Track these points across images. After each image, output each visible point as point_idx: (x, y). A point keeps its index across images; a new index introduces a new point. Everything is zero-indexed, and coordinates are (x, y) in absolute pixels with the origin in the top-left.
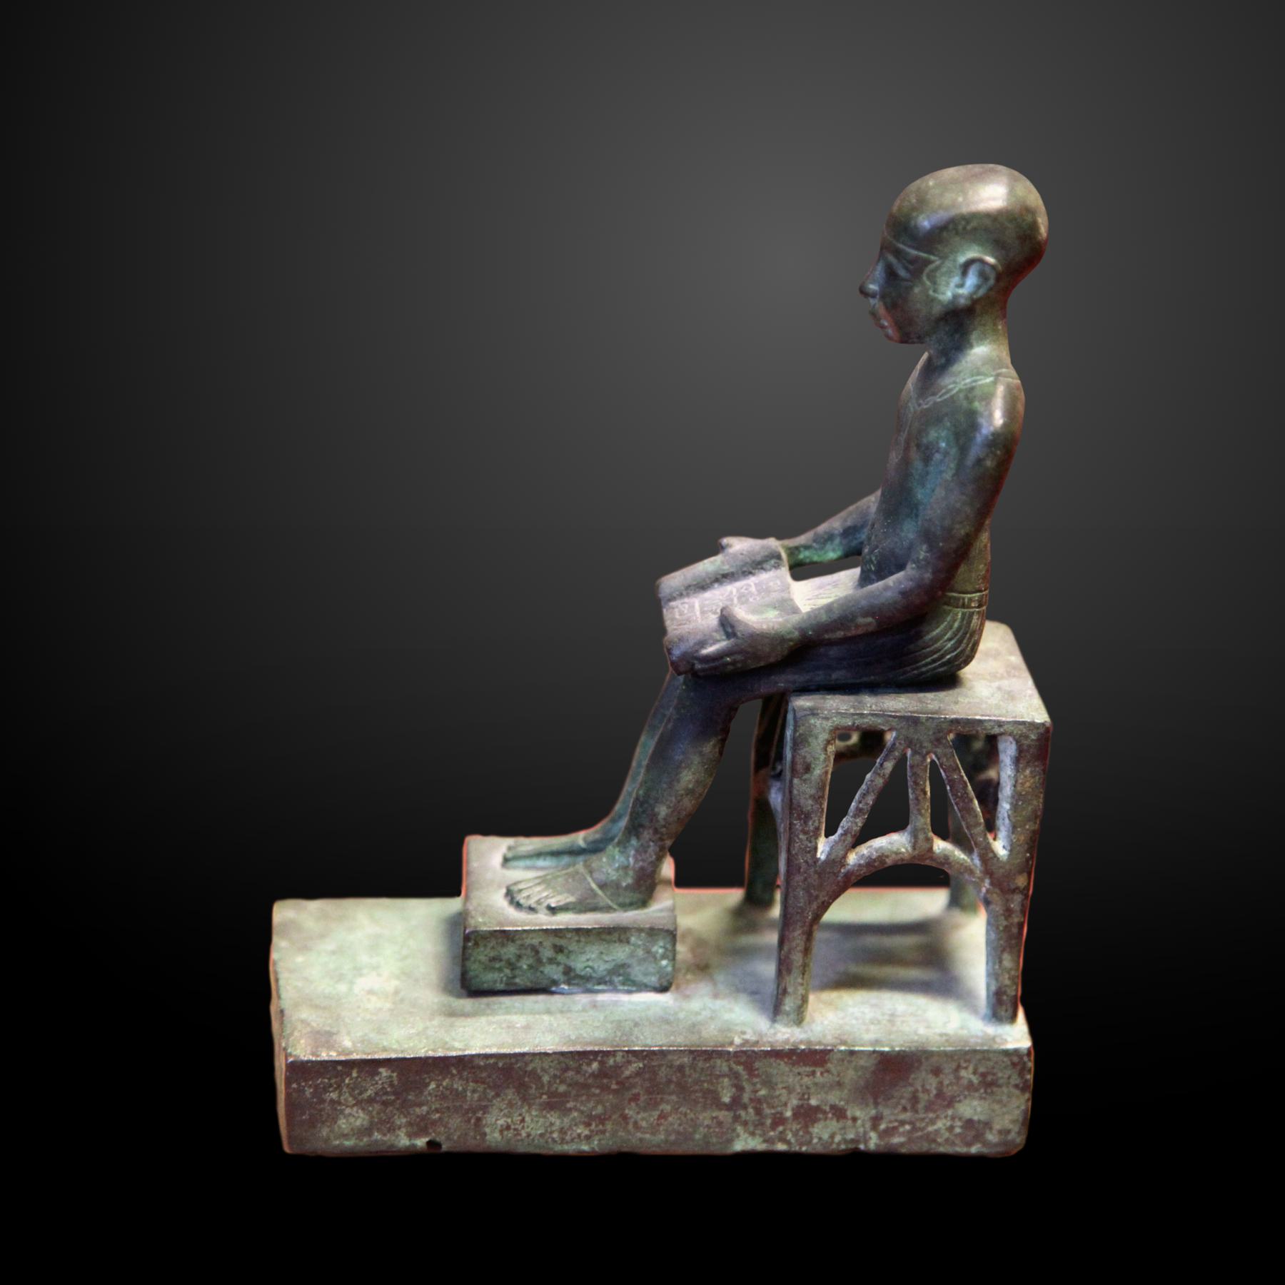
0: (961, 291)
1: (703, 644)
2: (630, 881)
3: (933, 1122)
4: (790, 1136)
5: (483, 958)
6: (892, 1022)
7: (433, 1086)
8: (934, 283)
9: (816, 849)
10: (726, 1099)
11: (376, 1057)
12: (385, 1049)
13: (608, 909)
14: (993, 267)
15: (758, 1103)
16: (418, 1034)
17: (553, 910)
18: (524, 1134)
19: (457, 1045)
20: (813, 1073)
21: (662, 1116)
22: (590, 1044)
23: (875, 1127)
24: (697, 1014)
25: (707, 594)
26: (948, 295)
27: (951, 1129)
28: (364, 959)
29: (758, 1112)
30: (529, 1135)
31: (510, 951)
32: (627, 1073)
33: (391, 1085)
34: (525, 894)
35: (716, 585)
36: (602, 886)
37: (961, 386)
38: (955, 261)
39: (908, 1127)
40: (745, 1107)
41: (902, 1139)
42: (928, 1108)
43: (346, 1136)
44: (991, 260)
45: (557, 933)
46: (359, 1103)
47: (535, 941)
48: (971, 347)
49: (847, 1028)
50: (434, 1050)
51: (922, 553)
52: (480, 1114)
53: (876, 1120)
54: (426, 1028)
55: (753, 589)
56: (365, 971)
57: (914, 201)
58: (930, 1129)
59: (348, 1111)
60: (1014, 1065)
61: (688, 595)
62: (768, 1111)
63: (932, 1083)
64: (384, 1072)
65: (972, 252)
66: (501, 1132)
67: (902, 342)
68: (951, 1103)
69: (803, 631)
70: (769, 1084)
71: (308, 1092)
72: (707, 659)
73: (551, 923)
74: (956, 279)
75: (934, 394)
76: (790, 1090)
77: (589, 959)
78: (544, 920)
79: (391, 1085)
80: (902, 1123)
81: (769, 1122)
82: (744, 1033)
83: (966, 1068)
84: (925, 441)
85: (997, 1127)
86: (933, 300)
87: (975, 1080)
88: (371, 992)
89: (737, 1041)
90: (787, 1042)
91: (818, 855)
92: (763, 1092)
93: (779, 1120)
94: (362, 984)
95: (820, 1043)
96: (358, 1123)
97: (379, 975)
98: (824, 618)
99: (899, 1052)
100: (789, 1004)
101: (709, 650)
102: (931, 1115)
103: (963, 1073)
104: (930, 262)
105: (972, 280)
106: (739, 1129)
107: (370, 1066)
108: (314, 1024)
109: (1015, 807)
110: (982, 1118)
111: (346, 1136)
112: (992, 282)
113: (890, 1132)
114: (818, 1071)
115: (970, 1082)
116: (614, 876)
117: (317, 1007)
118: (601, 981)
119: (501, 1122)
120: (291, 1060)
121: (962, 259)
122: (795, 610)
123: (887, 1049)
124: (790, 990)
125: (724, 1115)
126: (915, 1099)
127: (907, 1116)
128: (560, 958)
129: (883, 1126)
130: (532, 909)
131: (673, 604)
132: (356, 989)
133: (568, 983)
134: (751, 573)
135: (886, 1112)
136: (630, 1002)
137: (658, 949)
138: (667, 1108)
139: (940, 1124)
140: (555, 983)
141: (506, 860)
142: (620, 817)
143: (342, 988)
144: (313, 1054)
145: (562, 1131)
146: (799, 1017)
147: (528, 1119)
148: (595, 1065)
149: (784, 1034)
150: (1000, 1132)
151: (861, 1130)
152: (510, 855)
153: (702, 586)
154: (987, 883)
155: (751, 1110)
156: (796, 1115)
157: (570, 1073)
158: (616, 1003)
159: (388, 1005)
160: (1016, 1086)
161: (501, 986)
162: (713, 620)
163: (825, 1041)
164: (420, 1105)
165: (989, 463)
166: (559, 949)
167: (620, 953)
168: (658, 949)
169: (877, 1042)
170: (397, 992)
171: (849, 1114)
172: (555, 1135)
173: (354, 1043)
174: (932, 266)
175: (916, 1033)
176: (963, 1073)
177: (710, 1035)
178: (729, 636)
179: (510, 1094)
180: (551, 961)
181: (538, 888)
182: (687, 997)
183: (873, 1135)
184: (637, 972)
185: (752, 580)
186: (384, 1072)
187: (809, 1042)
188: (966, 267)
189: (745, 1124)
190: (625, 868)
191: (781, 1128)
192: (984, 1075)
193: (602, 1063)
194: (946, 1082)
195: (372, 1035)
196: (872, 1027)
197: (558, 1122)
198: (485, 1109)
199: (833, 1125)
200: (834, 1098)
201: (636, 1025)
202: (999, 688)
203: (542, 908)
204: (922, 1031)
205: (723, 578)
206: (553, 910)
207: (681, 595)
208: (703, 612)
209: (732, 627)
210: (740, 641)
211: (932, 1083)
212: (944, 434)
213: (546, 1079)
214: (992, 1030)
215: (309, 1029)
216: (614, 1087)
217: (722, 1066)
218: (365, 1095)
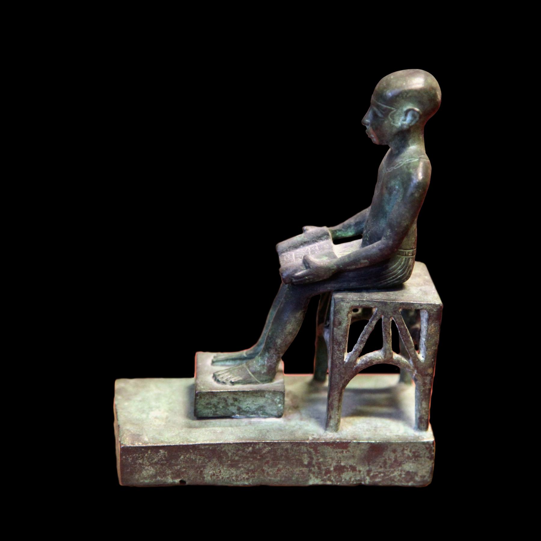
0: (404, 123)
1: (296, 271)
2: (265, 371)
3: (393, 472)
4: (332, 478)
5: (203, 403)
6: (375, 430)
7: (182, 457)
8: (393, 119)
9: (343, 357)
10: (306, 463)
11: (158, 445)
12: (162, 442)
13: (256, 383)
14: (418, 112)
15: (319, 464)
16: (176, 435)
17: (233, 383)
18: (221, 477)
19: (192, 440)
20: (342, 452)
21: (279, 470)
22: (248, 439)
23: (368, 475)
24: (294, 427)
25: (298, 250)
26: (399, 124)
27: (400, 475)
28: (153, 404)
29: (319, 468)
30: (223, 478)
31: (215, 400)
32: (264, 452)
33: (165, 457)
34: (221, 376)
35: (301, 246)
36: (254, 373)
37: (405, 162)
38: (402, 110)
39: (382, 475)
40: (314, 466)
41: (380, 480)
42: (391, 467)
43: (145, 478)
44: (417, 109)
45: (234, 393)
46: (151, 464)
47: (225, 396)
48: (409, 146)
49: (357, 433)
50: (183, 442)
51: (388, 233)
52: (202, 469)
53: (369, 472)
54: (179, 433)
55: (317, 248)
56: (154, 409)
57: (385, 84)
58: (392, 475)
59: (146, 468)
60: (427, 448)
61: (290, 251)
62: (323, 468)
63: (392, 456)
64: (162, 451)
65: (409, 106)
66: (211, 476)
68: (400, 464)
69: (338, 266)
70: (324, 456)
71: (130, 460)
72: (298, 277)
73: (232, 389)
74: (403, 118)
75: (393, 166)
76: (332, 459)
77: (248, 404)
78: (229, 387)
79: (165, 457)
80: (380, 473)
81: (324, 472)
82: (313, 435)
83: (407, 450)
84: (389, 186)
85: (420, 474)
86: (393, 126)
87: (411, 454)
88: (156, 418)
89: (310, 438)
90: (331, 438)
91: (345, 360)
92: (321, 460)
93: (328, 472)
94: (153, 414)
95: (345, 439)
96: (151, 473)
97: (160, 411)
98: (347, 260)
99: (378, 443)
100: (332, 423)
101: (299, 274)
102: (392, 469)
103: (405, 452)
104: (392, 110)
105: (409, 118)
106: (311, 475)
107: (156, 449)
108: (132, 431)
109: (427, 340)
110: (414, 471)
111: (145, 478)
112: (418, 119)
113: (375, 476)
114: (345, 451)
115: (409, 455)
116: (258, 369)
117: (133, 424)
118: (253, 413)
119: (211, 472)
120: (122, 446)
121: (405, 109)
122: (335, 257)
123: (373, 442)
124: (333, 417)
125: (305, 470)
126: (385, 463)
127: (382, 470)
128: (236, 403)
129: (372, 474)
130: (224, 383)
131: (283, 254)
132: (150, 417)
133: (239, 414)
134: (316, 241)
135: (373, 468)
136: (265, 422)
137: (277, 400)
138: (281, 466)
139: (396, 473)
140: (234, 414)
141: (213, 362)
143: (144, 416)
144: (132, 444)
145: (237, 476)
146: (336, 428)
147: (222, 471)
148: (251, 449)
149: (330, 435)
150: (421, 477)
151: (363, 476)
152: (215, 360)
153: (296, 247)
154: (415, 372)
155: (316, 468)
156: (335, 469)
157: (240, 452)
158: (259, 422)
159: (163, 423)
160: (428, 457)
161: (211, 415)
162: (300, 261)
163: (347, 438)
164: (177, 465)
165: (416, 195)
166: (235, 400)
167: (261, 401)
168: (277, 400)
169: (369, 439)
170: (167, 418)
171: (357, 469)
172: (234, 478)
173: (149, 439)
174: (392, 112)
175: (385, 435)
176: (405, 452)
177: (299, 436)
178: (307, 268)
179: (215, 460)
180: (232, 405)
181: (227, 374)
182: (289, 420)
183: (368, 478)
184: (268, 409)
185: (316, 244)
186: (162, 451)
187: (341, 439)
188: (407, 113)
189: (314, 473)
190: (263, 365)
191: (329, 475)
192: (414, 453)
193: (253, 448)
194: (398, 456)
195: (157, 436)
196: (367, 432)
197: (235, 473)
198: (204, 467)
199: (351, 474)
200: (351, 462)
201: (268, 431)
202: (421, 290)
203: (228, 382)
204: (388, 434)
205: (304, 243)
206: (233, 383)
207: (287, 251)
208: (296, 258)
209: (308, 264)
210: (311, 270)
211: (392, 456)
212: (397, 183)
213: (230, 454)
214: (417, 434)
215: (130, 433)
216: (259, 457)
217: (304, 449)
218: (154, 461)
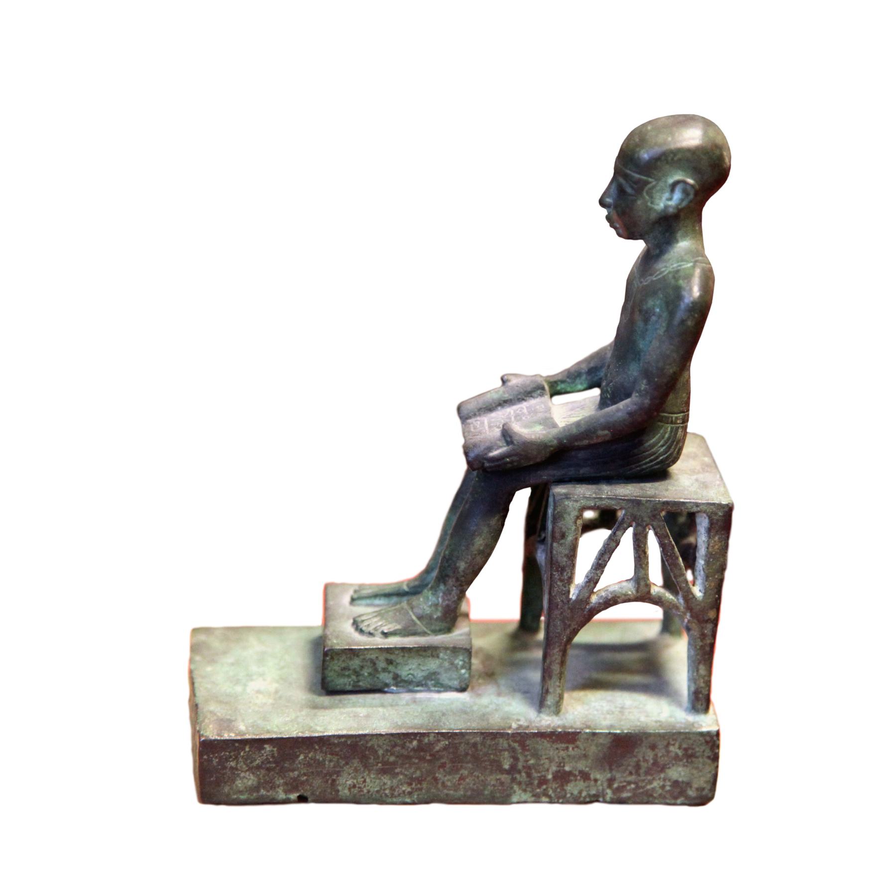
0: (670, 203)
1: (490, 449)
2: (439, 614)
3: (650, 782)
5: (336, 668)
6: (622, 712)
7: (302, 757)
8: (652, 197)
9: (569, 592)
10: (506, 767)
11: (262, 737)
12: (268, 732)
13: (424, 634)
14: (692, 186)
15: (528, 769)
16: (291, 721)
17: (385, 635)
18: (365, 791)
19: (319, 728)
20: (567, 748)
21: (462, 778)
22: (411, 728)
23: (610, 786)
24: (486, 707)
25: (493, 415)
26: (661, 205)
27: (663, 787)
28: (254, 668)
29: (529, 775)
30: (369, 792)
31: (356, 663)
32: (437, 748)
33: (273, 756)
34: (366, 623)
35: (499, 408)
36: (420, 618)
37: (670, 269)
38: (666, 182)
39: (633, 786)
40: (519, 772)
41: (629, 795)
42: (647, 773)
43: (241, 792)
44: (691, 181)
45: (388, 650)
46: (250, 769)
48: (677, 242)
49: (591, 717)
50: (302, 732)
51: (643, 385)
52: (334, 777)
53: (611, 781)
54: (297, 717)
55: (525, 411)
56: (255, 677)
57: (637, 140)
58: (649, 787)
59: (242, 775)
60: (707, 742)
61: (480, 415)
62: (535, 775)
63: (650, 755)
64: (268, 747)
65: (678, 176)
66: (349, 789)
68: (663, 769)
69: (560, 440)
70: (536, 756)
71: (215, 761)
72: (493, 459)
73: (384, 644)
74: (667, 195)
75: (651, 275)
76: (551, 760)
77: (411, 669)
78: (379, 642)
79: (273, 756)
80: (629, 783)
81: (536, 782)
82: (518, 720)
83: (674, 745)
84: (645, 307)
85: (695, 786)
86: (651, 209)
87: (680, 753)
88: (258, 692)
89: (514, 726)
90: (549, 726)
91: (571, 596)
92: (532, 762)
94: (253, 686)
95: (571, 727)
96: (250, 783)
97: (264, 680)
98: (575, 431)
99: (627, 734)
100: (550, 700)
101: (495, 453)
102: (649, 778)
103: (671, 748)
104: (648, 183)
105: (677, 195)
106: (516, 787)
107: (258, 743)
108: (219, 714)
109: (707, 563)
110: (685, 779)
111: (241, 792)
112: (691, 196)
114: (571, 747)
115: (677, 754)
116: (428, 611)
117: (221, 702)
118: (419, 684)
119: (349, 782)
120: (203, 739)
121: (671, 181)
122: (555, 425)
123: (618, 731)
124: (551, 690)
125: (505, 778)
126: (638, 766)
127: (632, 778)
128: (391, 668)
129: (615, 785)
130: (371, 634)
132: (249, 690)
133: (396, 685)
134: (523, 400)
135: (618, 775)
136: (439, 699)
137: (459, 662)
138: (465, 772)
139: (655, 784)
140: (387, 685)
141: (353, 600)
143: (239, 689)
144: (218, 735)
145: (392, 789)
146: (557, 709)
147: (368, 780)
148: (415, 743)
149: (547, 721)
150: (697, 789)
151: (601, 788)
152: (355, 596)
154: (688, 616)
155: (524, 774)
156: (555, 777)
157: (398, 749)
158: (429, 699)
159: (271, 701)
160: (709, 757)
161: (349, 688)
163: (575, 726)
164: (293, 770)
165: (689, 323)
166: (390, 662)
167: (432, 665)
168: (459, 662)
169: (611, 727)
170: (277, 692)
171: (592, 777)
172: (387, 792)
173: (247, 727)
174: (650, 186)
175: (638, 720)
176: (671, 748)
177: (495, 722)
178: (508, 443)
179: (356, 763)
180: (385, 670)
181: (375, 620)
182: (479, 695)
184: (444, 678)
185: (524, 405)
186: (268, 747)
187: (564, 727)
188: (673, 186)
189: (520, 783)
190: (436, 605)
191: (544, 787)
192: (686, 750)
193: (420, 741)
194: (660, 755)
195: (259, 722)
196: (608, 716)
197: (389, 783)
198: (338, 773)
199: (581, 784)
200: (582, 765)
201: (444, 714)
202: (697, 480)
203: (378, 633)
204: (643, 719)
206: (385, 635)
207: (475, 415)
208: (490, 427)
209: (511, 437)
210: (516, 447)
211: (650, 755)
212: (658, 302)
213: (381, 752)
214: (691, 718)
215: (215, 718)
216: (428, 758)
217: (503, 743)
218: (255, 764)
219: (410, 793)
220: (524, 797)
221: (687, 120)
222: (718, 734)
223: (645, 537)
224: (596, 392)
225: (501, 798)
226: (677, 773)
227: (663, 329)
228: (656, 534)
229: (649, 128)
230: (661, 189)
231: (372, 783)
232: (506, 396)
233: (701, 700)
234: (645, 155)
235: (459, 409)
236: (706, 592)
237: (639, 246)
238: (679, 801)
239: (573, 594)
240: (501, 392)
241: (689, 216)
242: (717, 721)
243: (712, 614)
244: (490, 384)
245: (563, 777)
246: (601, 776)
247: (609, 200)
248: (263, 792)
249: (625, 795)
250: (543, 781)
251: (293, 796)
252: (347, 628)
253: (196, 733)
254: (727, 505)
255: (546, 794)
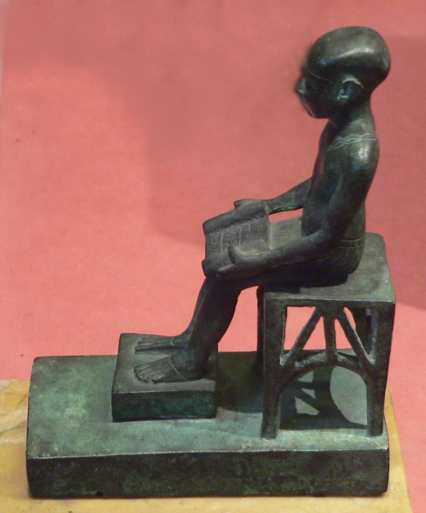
1: (219, 265)
2: (192, 368)
7: (96, 470)
9: (279, 360)
10: (239, 473)
12: (73, 453)
13: (182, 380)
16: (90, 443)
17: (155, 382)
18: (142, 489)
19: (108, 450)
20: (281, 462)
22: (170, 450)
23: (312, 484)
27: (350, 485)
29: (255, 479)
30: (144, 490)
34: (142, 373)
35: (232, 225)
36: (179, 370)
37: (345, 143)
38: (340, 82)
39: (328, 484)
41: (326, 489)
45: (156, 394)
49: (299, 438)
50: (96, 454)
53: (312, 482)
54: (95, 440)
56: (70, 404)
57: (319, 50)
58: (341, 485)
59: (57, 481)
61: (218, 230)
64: (73, 464)
67: (116, 398)
68: (349, 474)
72: (221, 273)
73: (153, 389)
74: (342, 91)
78: (152, 388)
81: (260, 483)
83: (356, 459)
87: (361, 463)
88: (71, 417)
89: (244, 447)
91: (281, 363)
94: (69, 411)
95: (284, 448)
97: (77, 406)
98: (279, 255)
99: (323, 452)
100: (269, 429)
101: (223, 269)
102: (341, 479)
103: (355, 461)
105: (349, 91)
106: (246, 486)
107: (67, 461)
108: (42, 437)
109: (378, 341)
116: (184, 365)
117: (44, 426)
119: (131, 484)
120: (29, 458)
123: (317, 450)
127: (328, 480)
129: (316, 484)
130: (145, 381)
134: (249, 220)
139: (344, 483)
141: (137, 351)
142: (134, 437)
143: (58, 414)
147: (143, 483)
148: (174, 460)
149: (268, 444)
152: (138, 349)
156: (275, 479)
159: (78, 425)
160: (381, 466)
163: (286, 447)
167: (188, 402)
169: (312, 446)
170: (83, 417)
171: (299, 479)
173: (59, 449)
176: (355, 461)
178: (233, 262)
181: (149, 370)
182: (222, 421)
183: (311, 487)
185: (249, 224)
186: (73, 464)
187: (278, 447)
189: (248, 484)
191: (266, 485)
194: (346, 465)
201: (196, 437)
202: (371, 280)
206: (155, 382)
207: (215, 230)
208: (224, 242)
209: (234, 258)
210: (236, 266)
214: (369, 439)
215: (39, 440)
219: (173, 491)
220: (252, 492)
221: (354, 33)
222: (388, 451)
223: (333, 325)
224: (300, 213)
225: (237, 493)
226: (359, 476)
227: (338, 196)
228: (340, 322)
229: (329, 40)
230: (336, 86)
231: (147, 485)
232: (237, 217)
233: (376, 426)
234: (323, 62)
235: (204, 225)
236: (378, 359)
237: (324, 122)
238: (361, 493)
239: (282, 361)
240: (234, 213)
241: (360, 102)
242: (388, 440)
243: (383, 373)
244: (226, 207)
245: (279, 480)
246: (306, 479)
247: (302, 91)
248: (72, 490)
249: (323, 490)
250: (265, 482)
251: (93, 493)
252: (131, 373)
253: (27, 456)
254: (391, 303)
255: (268, 490)
